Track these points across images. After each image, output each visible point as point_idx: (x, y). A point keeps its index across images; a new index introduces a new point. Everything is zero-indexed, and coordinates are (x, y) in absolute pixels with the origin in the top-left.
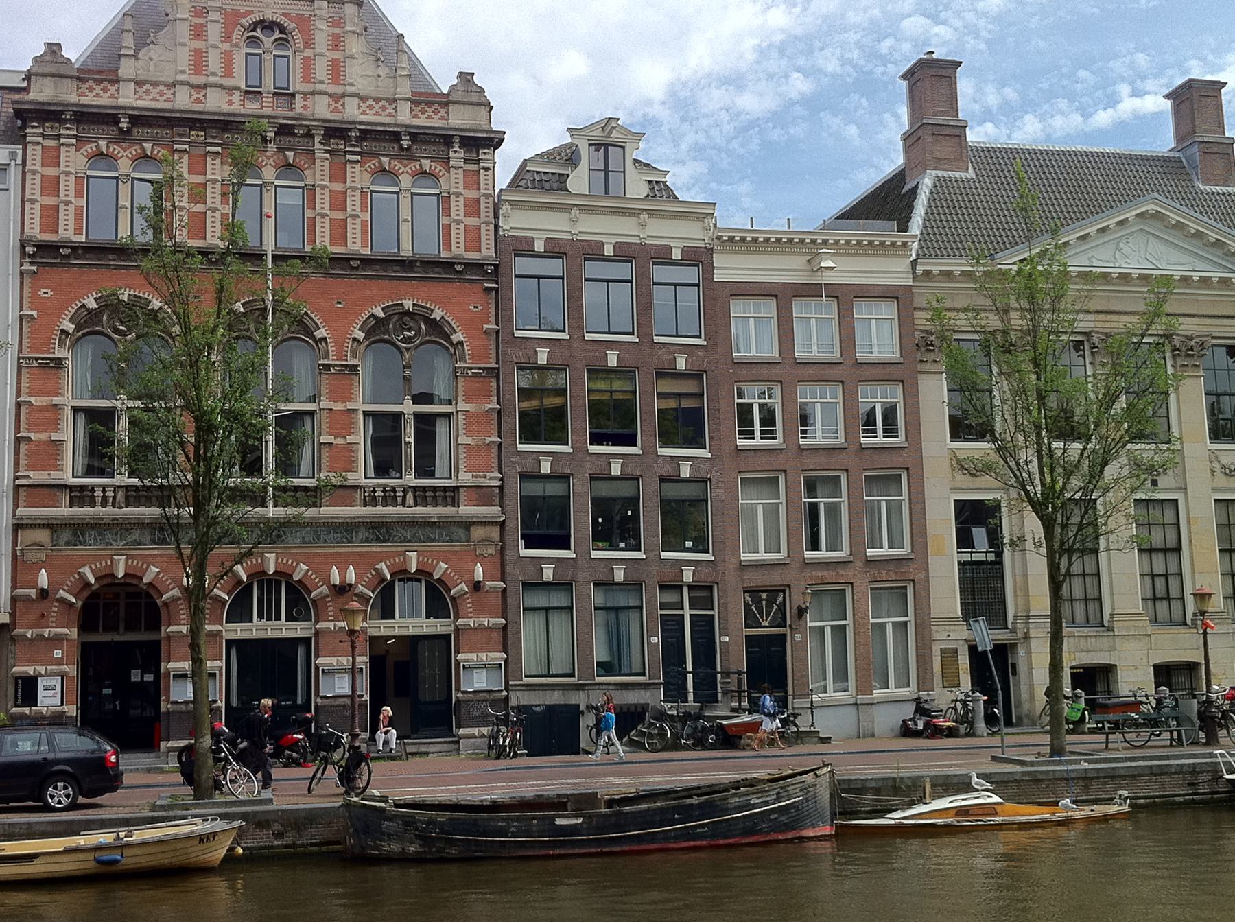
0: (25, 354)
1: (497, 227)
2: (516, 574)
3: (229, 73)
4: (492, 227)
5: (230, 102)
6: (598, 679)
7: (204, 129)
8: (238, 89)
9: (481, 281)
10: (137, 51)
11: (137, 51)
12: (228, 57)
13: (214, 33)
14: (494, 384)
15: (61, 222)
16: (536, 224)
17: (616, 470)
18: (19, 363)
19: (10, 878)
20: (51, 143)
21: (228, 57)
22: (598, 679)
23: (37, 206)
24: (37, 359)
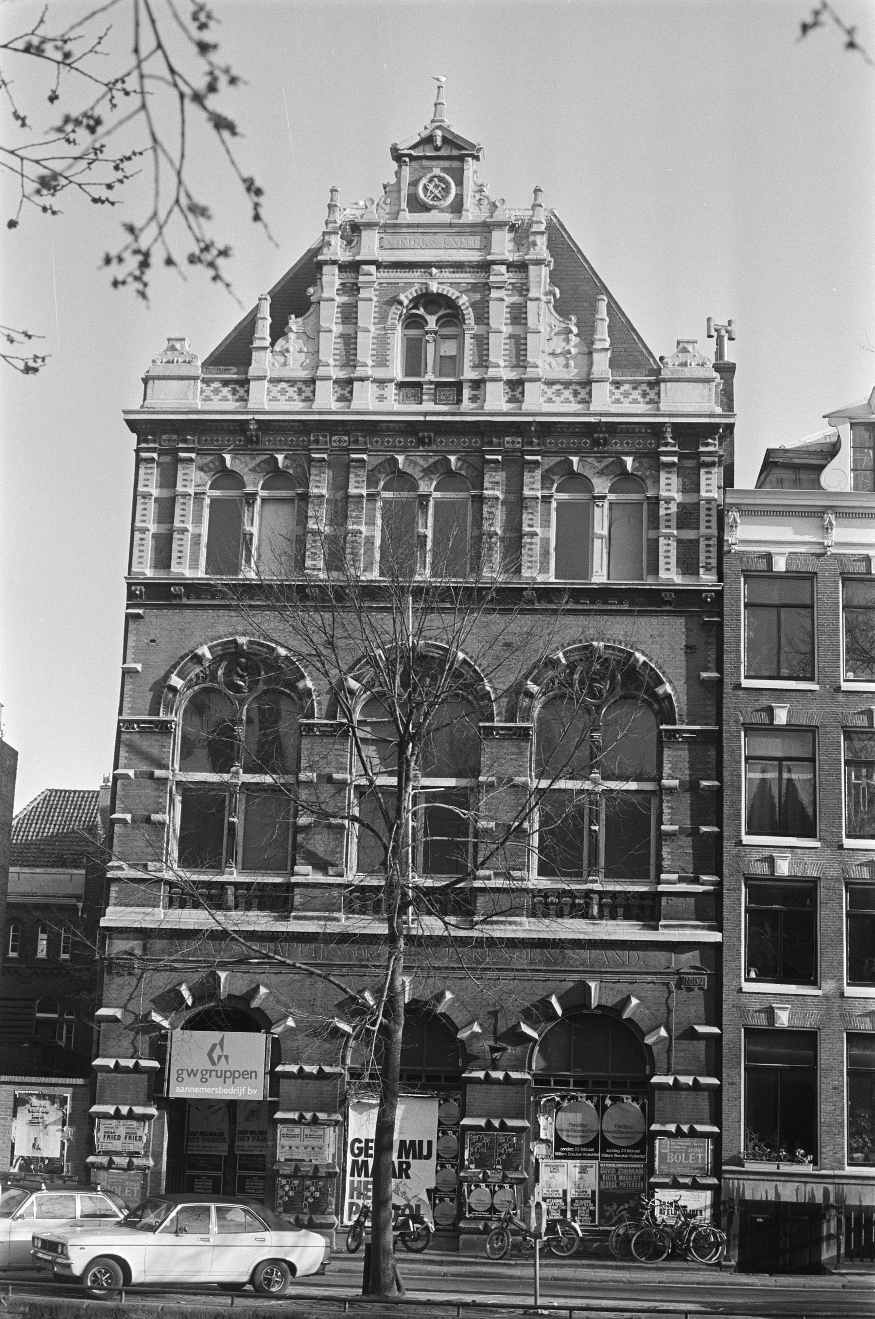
0: (125, 717)
1: (721, 541)
2: (736, 710)
3: (382, 361)
4: (714, 541)
5: (381, 398)
6: (849, 1170)
7: (347, 433)
8: (391, 381)
9: (699, 614)
10: (273, 344)
11: (273, 344)
12: (382, 343)
13: (367, 314)
14: (712, 753)
15: (175, 555)
16: (770, 538)
17: (781, 717)
18: (119, 727)
19: (859, 521)
20: (166, 459)
21: (382, 343)
22: (849, 1170)
23: (149, 536)
24: (138, 722)
